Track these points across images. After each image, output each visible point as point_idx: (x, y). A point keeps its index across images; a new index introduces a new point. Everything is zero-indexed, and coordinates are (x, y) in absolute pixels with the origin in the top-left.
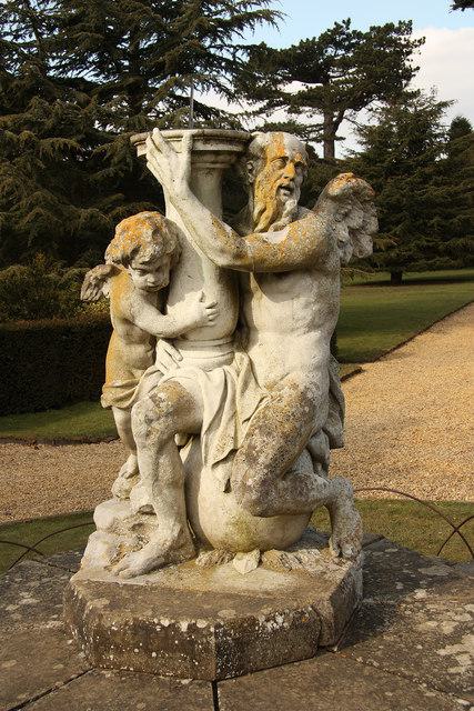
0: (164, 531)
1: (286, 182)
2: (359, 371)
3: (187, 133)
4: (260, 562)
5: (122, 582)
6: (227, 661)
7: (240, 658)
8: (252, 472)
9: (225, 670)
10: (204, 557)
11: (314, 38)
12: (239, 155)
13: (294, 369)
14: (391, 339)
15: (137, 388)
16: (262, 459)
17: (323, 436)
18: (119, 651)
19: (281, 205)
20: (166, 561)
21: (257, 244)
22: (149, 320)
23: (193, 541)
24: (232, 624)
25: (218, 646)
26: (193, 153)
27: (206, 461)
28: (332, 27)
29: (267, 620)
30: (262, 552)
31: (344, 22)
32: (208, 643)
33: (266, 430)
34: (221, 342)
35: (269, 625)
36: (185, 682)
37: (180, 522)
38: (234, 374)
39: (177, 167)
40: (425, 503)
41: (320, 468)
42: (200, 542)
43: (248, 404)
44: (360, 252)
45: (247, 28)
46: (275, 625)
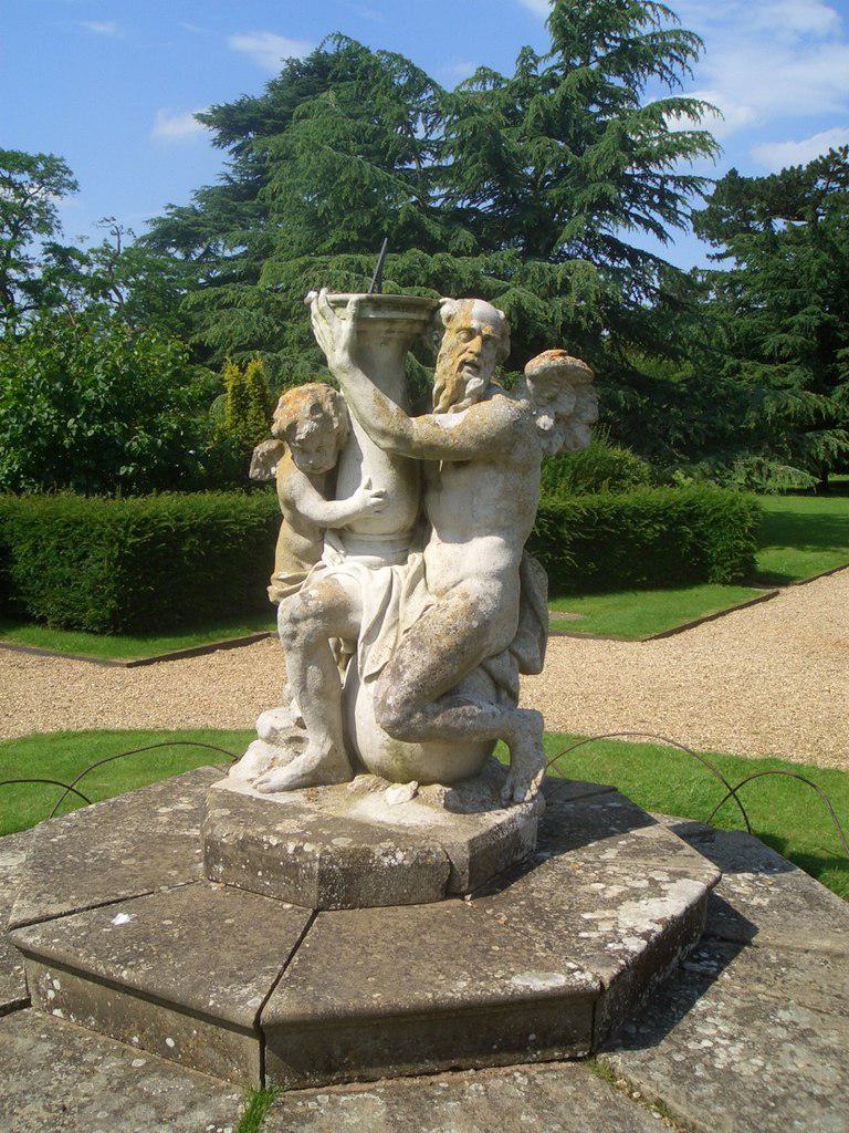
0: (316, 747)
1: (470, 357)
2: (776, 594)
3: (353, 297)
4: (416, 794)
5: (257, 795)
6: (332, 891)
7: (347, 891)
8: (394, 689)
9: (330, 901)
10: (359, 780)
11: (801, 166)
12: (426, 324)
13: (468, 576)
14: (807, 556)
15: (307, 581)
16: (407, 676)
17: (507, 657)
18: (227, 865)
19: (462, 383)
20: (313, 780)
21: (426, 426)
22: (315, 506)
23: (347, 762)
24: (342, 853)
25: (321, 873)
26: (359, 319)
27: (361, 673)
28: (826, 154)
29: (385, 855)
30: (419, 786)
31: (840, 149)
32: (311, 868)
33: (418, 643)
34: (360, 537)
35: (386, 861)
36: (288, 906)
37: (333, 738)
38: (402, 575)
39: (339, 336)
40: (700, 757)
41: (504, 695)
42: (357, 765)
43: (411, 611)
44: (576, 445)
45: (680, 158)
46: (393, 861)
